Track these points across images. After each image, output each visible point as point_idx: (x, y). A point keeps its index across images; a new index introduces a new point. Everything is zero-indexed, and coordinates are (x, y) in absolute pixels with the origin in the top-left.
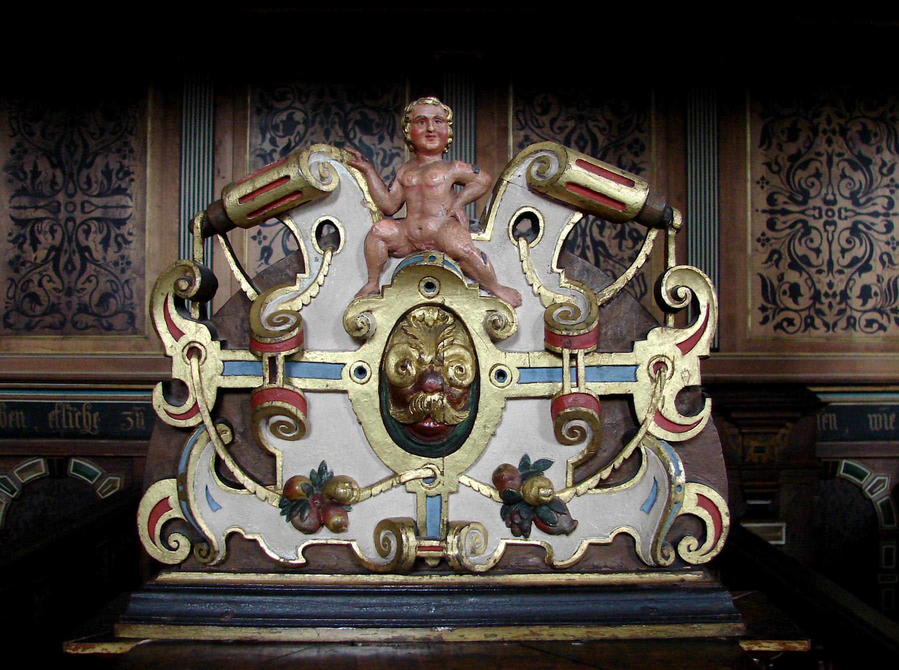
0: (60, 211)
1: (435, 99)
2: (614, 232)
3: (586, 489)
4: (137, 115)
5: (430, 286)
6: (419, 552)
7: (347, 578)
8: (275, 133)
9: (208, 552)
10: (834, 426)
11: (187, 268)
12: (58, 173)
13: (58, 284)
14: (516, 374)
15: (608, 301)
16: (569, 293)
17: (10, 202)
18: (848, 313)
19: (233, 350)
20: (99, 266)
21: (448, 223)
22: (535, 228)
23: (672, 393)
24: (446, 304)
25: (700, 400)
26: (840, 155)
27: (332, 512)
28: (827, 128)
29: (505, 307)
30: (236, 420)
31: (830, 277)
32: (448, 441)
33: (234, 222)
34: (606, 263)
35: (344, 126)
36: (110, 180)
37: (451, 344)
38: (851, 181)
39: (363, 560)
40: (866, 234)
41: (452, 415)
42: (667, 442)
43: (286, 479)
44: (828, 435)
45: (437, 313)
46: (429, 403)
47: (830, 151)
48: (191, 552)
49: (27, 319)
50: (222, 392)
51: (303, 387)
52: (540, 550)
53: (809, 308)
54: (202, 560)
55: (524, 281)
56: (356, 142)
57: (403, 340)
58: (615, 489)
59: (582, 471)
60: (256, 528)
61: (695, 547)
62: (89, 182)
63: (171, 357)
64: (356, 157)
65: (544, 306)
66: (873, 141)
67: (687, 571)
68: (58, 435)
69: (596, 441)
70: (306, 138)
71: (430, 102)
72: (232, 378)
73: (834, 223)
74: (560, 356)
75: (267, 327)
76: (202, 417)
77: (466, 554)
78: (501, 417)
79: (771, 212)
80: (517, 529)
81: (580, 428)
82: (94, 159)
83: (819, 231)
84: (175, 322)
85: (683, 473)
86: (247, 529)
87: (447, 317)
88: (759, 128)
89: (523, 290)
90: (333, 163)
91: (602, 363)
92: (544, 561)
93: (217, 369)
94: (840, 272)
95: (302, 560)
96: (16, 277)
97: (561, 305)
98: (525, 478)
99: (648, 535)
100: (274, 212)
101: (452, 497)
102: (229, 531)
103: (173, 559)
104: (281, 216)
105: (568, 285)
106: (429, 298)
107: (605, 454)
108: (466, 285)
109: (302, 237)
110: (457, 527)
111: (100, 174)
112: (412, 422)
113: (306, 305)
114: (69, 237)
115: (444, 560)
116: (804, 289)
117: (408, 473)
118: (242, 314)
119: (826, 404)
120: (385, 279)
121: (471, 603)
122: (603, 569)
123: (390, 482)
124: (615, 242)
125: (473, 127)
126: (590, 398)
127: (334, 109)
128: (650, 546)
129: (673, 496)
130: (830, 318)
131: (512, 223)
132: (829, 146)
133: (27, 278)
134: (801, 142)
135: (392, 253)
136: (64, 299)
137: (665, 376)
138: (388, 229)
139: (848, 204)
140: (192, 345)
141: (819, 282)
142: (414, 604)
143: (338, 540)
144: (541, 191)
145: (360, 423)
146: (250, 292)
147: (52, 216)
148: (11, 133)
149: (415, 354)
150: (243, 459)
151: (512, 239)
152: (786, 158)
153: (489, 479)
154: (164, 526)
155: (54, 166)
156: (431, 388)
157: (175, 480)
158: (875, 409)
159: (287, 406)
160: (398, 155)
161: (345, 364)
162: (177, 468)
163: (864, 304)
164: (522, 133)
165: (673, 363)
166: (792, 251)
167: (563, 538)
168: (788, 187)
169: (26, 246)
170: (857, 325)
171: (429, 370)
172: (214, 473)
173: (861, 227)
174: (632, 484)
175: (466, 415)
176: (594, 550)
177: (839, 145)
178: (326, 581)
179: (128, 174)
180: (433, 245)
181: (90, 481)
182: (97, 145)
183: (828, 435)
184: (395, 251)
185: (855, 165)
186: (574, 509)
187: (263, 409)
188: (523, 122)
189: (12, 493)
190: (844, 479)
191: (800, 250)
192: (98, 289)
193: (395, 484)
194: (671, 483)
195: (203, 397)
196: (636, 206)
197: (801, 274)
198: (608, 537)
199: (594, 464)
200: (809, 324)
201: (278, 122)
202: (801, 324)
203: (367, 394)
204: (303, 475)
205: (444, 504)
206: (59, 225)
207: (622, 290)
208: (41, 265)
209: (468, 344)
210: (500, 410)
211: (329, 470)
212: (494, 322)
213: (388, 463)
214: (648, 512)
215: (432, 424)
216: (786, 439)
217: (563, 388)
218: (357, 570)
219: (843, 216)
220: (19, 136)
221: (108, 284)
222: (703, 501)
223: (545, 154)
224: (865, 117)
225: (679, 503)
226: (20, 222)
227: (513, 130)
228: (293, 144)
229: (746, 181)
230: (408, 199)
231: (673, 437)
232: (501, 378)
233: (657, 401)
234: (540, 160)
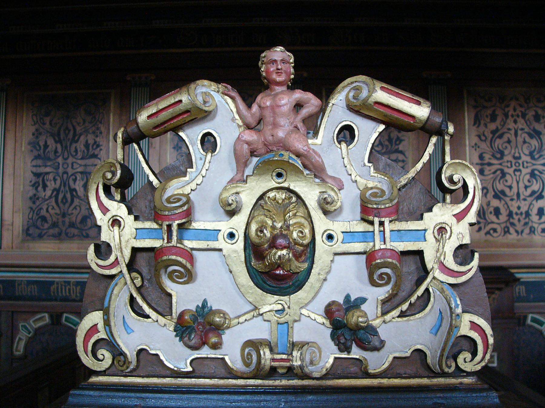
0: (59, 168)
1: (282, 48)
3: (391, 318)
4: (104, 112)
5: (279, 175)
6: (272, 363)
7: (221, 382)
9: (124, 363)
10: (523, 293)
11: (112, 165)
12: (59, 146)
13: (58, 211)
14: (341, 237)
15: (404, 186)
16: (376, 180)
17: (31, 163)
18: (530, 224)
19: (143, 221)
20: (81, 200)
21: (292, 131)
22: (353, 136)
23: (451, 249)
24: (291, 188)
25: (470, 255)
26: (522, 129)
27: (211, 335)
28: (514, 113)
29: (333, 189)
30: (144, 270)
32: (292, 284)
33: (144, 133)
36: (88, 150)
37: (295, 215)
38: (529, 145)
39: (233, 369)
40: (539, 176)
41: (296, 266)
42: (448, 284)
43: (179, 312)
44: (520, 299)
45: (285, 194)
46: (280, 257)
47: (516, 127)
48: (113, 362)
50: (135, 251)
51: (191, 247)
52: (358, 362)
53: (506, 222)
54: (120, 368)
55: (345, 172)
57: (261, 213)
58: (412, 318)
59: (388, 306)
60: (158, 346)
61: (470, 360)
62: (76, 151)
63: (100, 227)
64: (228, 89)
65: (359, 189)
67: (464, 377)
68: (56, 300)
69: (398, 283)
71: (278, 50)
72: (142, 241)
73: (520, 170)
74: (372, 223)
75: (166, 204)
76: (121, 268)
77: (306, 364)
78: (331, 267)
80: (342, 347)
81: (386, 274)
83: (511, 176)
84: (103, 202)
85: (460, 306)
86: (152, 347)
87: (292, 197)
88: (473, 115)
89: (345, 179)
90: (212, 93)
91: (401, 229)
92: (361, 370)
93: (131, 234)
94: (525, 200)
95: (190, 369)
96: (34, 207)
97: (372, 188)
98: (348, 310)
99: (436, 351)
100: (171, 127)
101: (296, 324)
102: (139, 348)
103: (100, 367)
104: (176, 129)
105: (376, 175)
106: (279, 183)
107: (404, 294)
108: (305, 174)
109: (191, 144)
110: (302, 345)
111: (83, 146)
112: (267, 270)
113: (194, 190)
114: (64, 183)
115: (290, 369)
116: (503, 211)
117: (265, 307)
118: (149, 197)
119: (518, 279)
120: (248, 171)
121: (310, 400)
122: (404, 376)
123: (252, 313)
126: (394, 253)
128: (438, 359)
129: (454, 323)
130: (519, 227)
131: (336, 132)
133: (40, 207)
135: (253, 153)
136: (61, 219)
137: (446, 237)
138: (250, 136)
139: (528, 159)
140: (115, 218)
141: (512, 206)
142: (269, 401)
143: (215, 354)
144: (356, 109)
145: (231, 272)
146: (155, 182)
147: (55, 171)
148: (33, 123)
149: (270, 222)
150: (149, 298)
151: (336, 143)
153: (322, 311)
154: (95, 344)
155: (56, 142)
156: (281, 245)
157: (102, 312)
159: (179, 259)
161: (220, 230)
162: (103, 304)
165: (451, 228)
167: (376, 353)
168: (491, 149)
169: (40, 188)
171: (279, 234)
172: (129, 307)
173: (536, 172)
174: (423, 314)
175: (306, 265)
176: (397, 362)
177: (521, 123)
178: (206, 384)
179: (98, 146)
180: (282, 147)
182: (81, 130)
183: (520, 299)
184: (255, 152)
185: (532, 135)
186: (383, 332)
187: (162, 261)
189: (29, 334)
190: (531, 326)
191: (500, 186)
192: (81, 214)
193: (255, 315)
194: (452, 313)
195: (122, 253)
196: (422, 118)
197: (500, 201)
198: (407, 352)
199: (396, 300)
200: (506, 231)
202: (501, 233)
203: (236, 251)
204: (191, 309)
205: (290, 330)
206: (59, 176)
207: (413, 178)
208: (47, 200)
209: (306, 215)
210: (330, 262)
211: (209, 305)
212: (325, 199)
213: (251, 300)
214: (436, 334)
215: (281, 272)
216: (495, 301)
217: (374, 246)
218: (229, 376)
220: (37, 126)
221: (87, 210)
222: (474, 326)
223: (359, 84)
224: (536, 106)
225: (458, 327)
229: (465, 145)
230: (264, 116)
231: (452, 281)
232: (330, 240)
233: (441, 255)
234: (356, 89)
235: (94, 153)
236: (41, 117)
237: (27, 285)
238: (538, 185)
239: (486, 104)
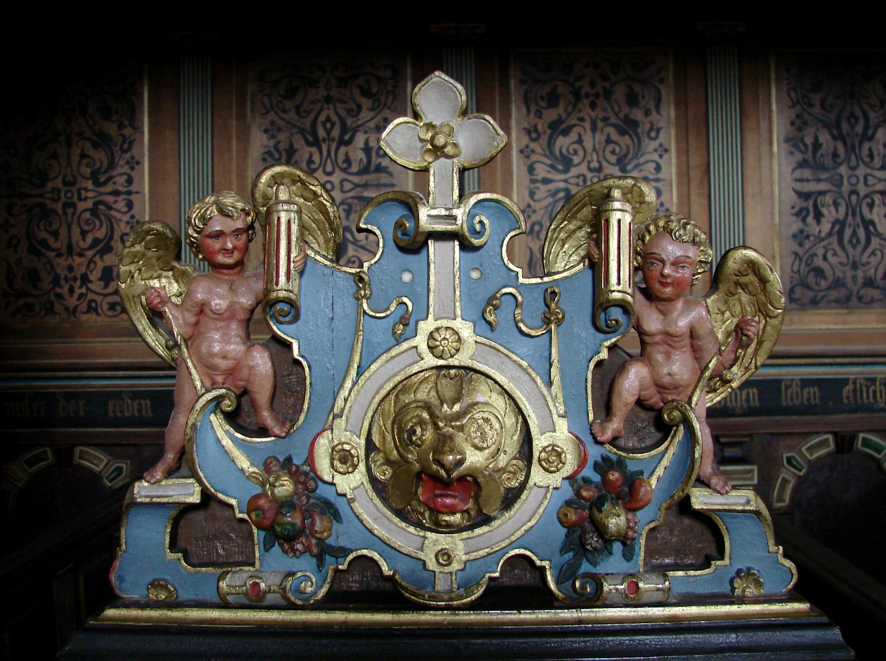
17: (792, 174)
26: (605, 119)
31: (70, 261)
49: (812, 294)
66: (115, 117)
73: (73, 205)
79: (129, 193)
82: (833, 228)
94: (81, 255)
96: (801, 251)
132: (593, 110)
134: (561, 107)
136: (849, 274)
147: (835, 189)
152: (546, 125)
155: (834, 138)
158: (117, 395)
163: (106, 286)
169: (810, 220)
181: (96, 468)
182: (878, 117)
206: (842, 197)
208: (823, 239)
220: (798, 108)
226: (801, 195)
236: (280, 99)
237: (802, 388)
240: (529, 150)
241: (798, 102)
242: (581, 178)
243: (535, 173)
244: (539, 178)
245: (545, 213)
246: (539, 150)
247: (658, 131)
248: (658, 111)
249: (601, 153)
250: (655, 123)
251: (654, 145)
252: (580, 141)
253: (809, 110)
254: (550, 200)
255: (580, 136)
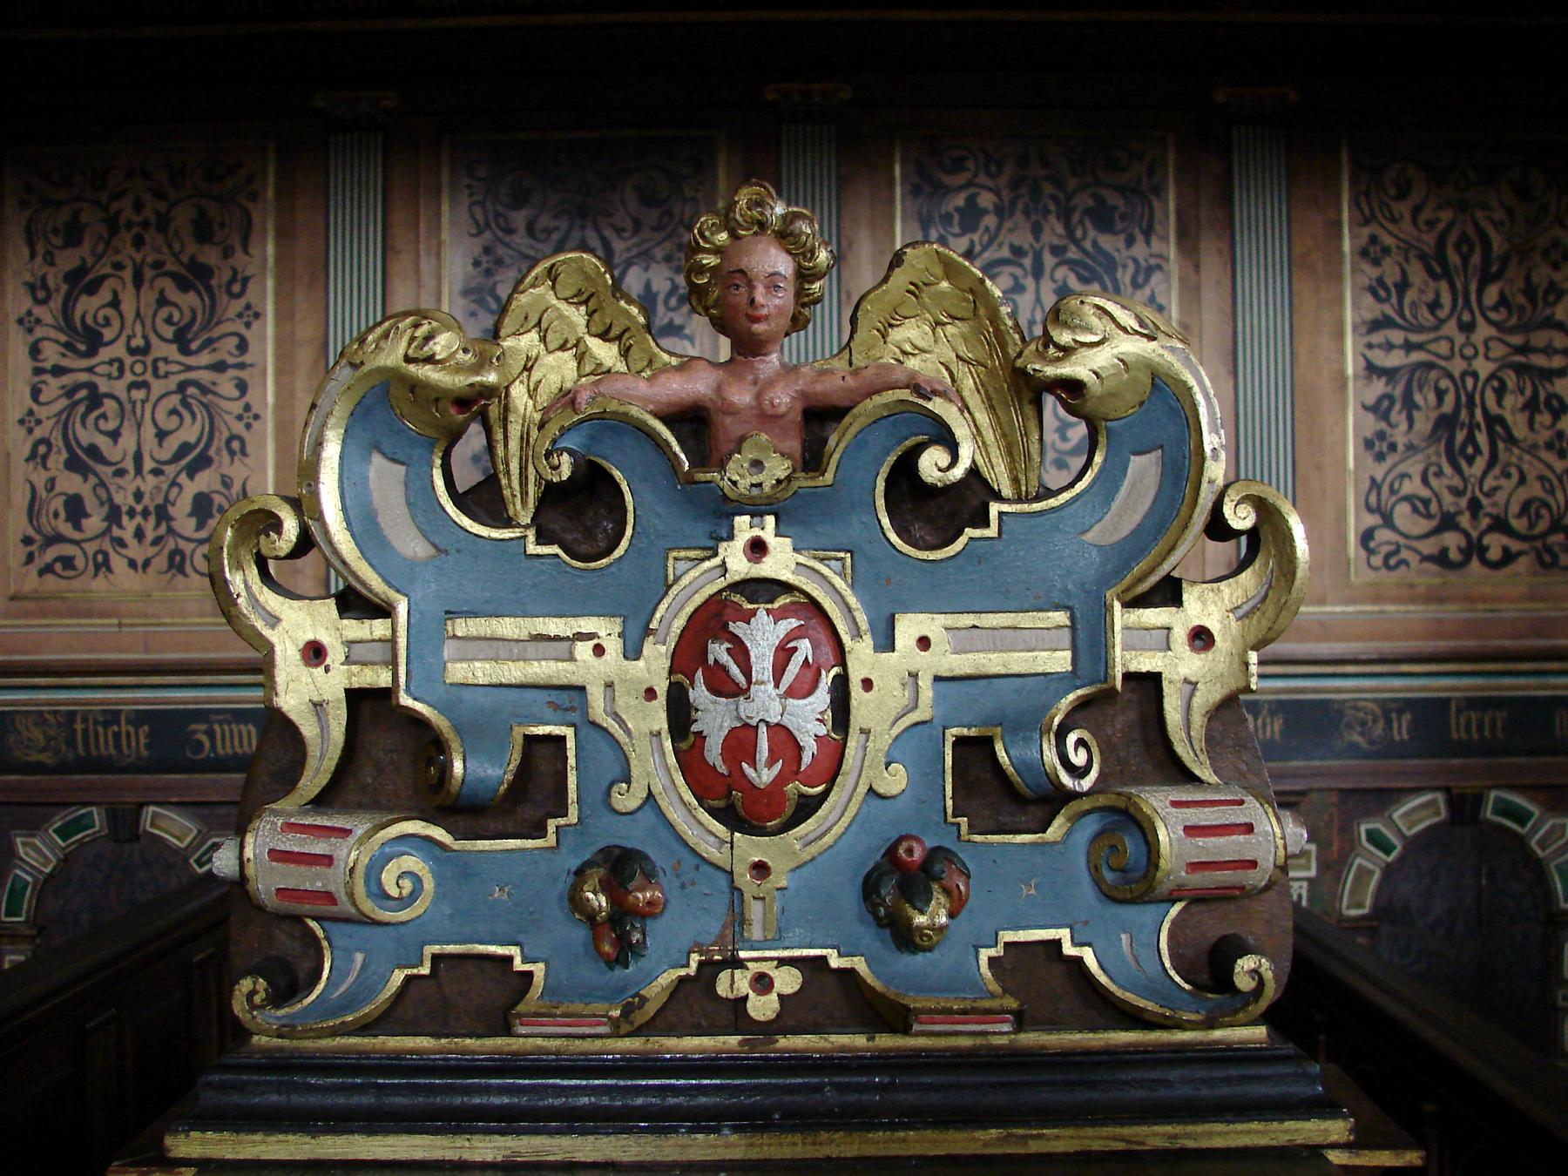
2: (1521, 401)
4: (699, 196)
8: (944, 228)
26: (157, 265)
34: (1508, 454)
35: (1065, 216)
56: (1088, 245)
70: (1000, 239)
116: (90, 503)
124: (1522, 418)
125: (1285, 224)
127: (1048, 188)
134: (85, 249)
139: (172, 351)
148: (474, 231)
152: (61, 276)
160: (1159, 267)
164: (1366, 232)
166: (71, 437)
169: (1398, 416)
170: (188, 563)
182: (629, 249)
188: (1367, 211)
201: (950, 209)
219: (162, 371)
220: (487, 235)
227: (1351, 225)
228: (978, 248)
235: (671, 322)
236: (500, 209)
238: (198, 426)
239: (948, 180)
240: (32, 319)
241: (488, 226)
242: (116, 365)
243: (41, 357)
244: (48, 365)
245: (57, 422)
246: (49, 319)
247: (246, 281)
248: (246, 250)
249: (148, 322)
250: (240, 270)
251: (237, 306)
252: (115, 303)
253: (507, 239)
254: (64, 402)
255: (115, 293)
